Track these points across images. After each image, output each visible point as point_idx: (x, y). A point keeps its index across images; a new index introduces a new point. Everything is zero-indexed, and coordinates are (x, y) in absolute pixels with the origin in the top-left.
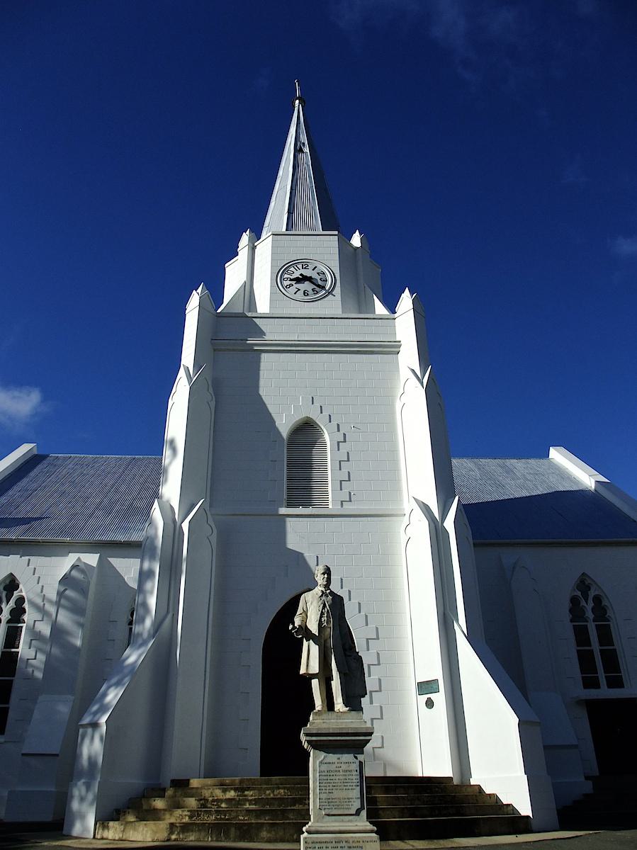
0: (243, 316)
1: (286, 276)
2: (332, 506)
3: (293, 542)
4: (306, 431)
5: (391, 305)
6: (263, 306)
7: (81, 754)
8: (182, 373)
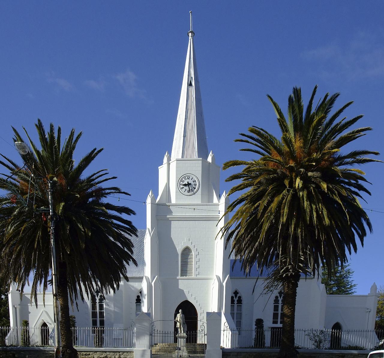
0: (164, 205)
1: (181, 183)
2: (193, 276)
3: (181, 287)
4: (187, 251)
5: (219, 197)
6: (173, 201)
7: (103, 307)
8: (147, 231)
